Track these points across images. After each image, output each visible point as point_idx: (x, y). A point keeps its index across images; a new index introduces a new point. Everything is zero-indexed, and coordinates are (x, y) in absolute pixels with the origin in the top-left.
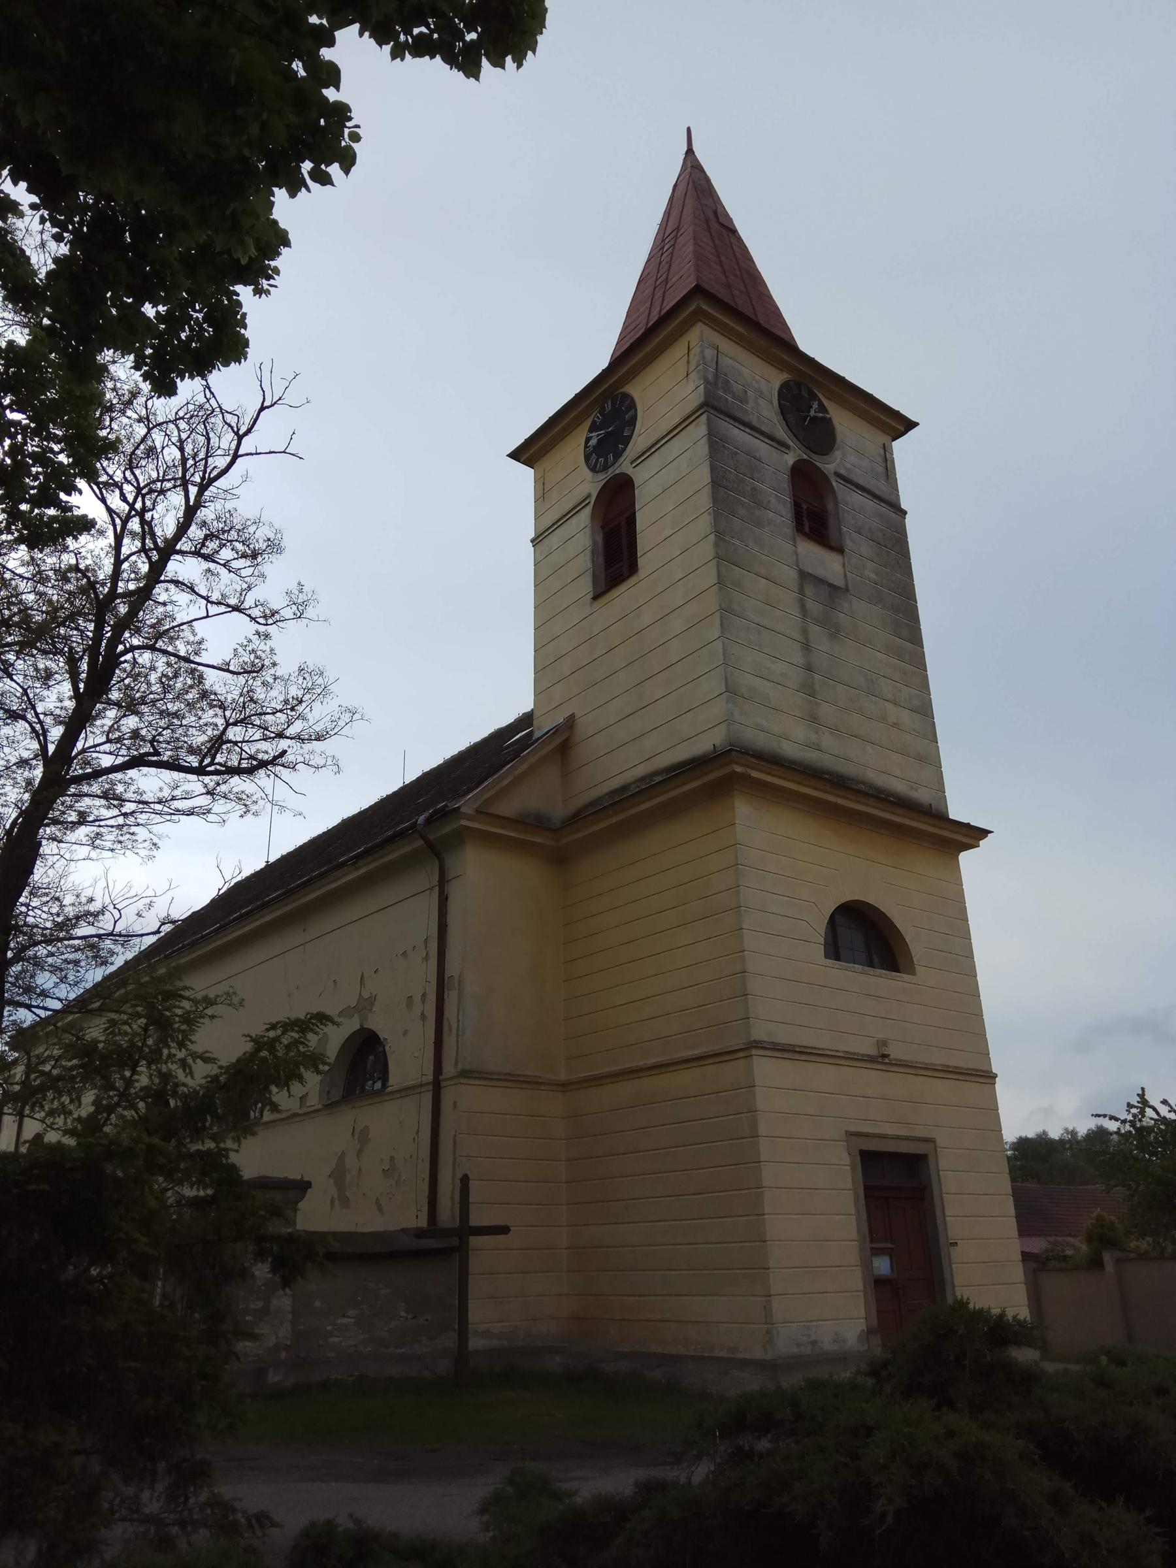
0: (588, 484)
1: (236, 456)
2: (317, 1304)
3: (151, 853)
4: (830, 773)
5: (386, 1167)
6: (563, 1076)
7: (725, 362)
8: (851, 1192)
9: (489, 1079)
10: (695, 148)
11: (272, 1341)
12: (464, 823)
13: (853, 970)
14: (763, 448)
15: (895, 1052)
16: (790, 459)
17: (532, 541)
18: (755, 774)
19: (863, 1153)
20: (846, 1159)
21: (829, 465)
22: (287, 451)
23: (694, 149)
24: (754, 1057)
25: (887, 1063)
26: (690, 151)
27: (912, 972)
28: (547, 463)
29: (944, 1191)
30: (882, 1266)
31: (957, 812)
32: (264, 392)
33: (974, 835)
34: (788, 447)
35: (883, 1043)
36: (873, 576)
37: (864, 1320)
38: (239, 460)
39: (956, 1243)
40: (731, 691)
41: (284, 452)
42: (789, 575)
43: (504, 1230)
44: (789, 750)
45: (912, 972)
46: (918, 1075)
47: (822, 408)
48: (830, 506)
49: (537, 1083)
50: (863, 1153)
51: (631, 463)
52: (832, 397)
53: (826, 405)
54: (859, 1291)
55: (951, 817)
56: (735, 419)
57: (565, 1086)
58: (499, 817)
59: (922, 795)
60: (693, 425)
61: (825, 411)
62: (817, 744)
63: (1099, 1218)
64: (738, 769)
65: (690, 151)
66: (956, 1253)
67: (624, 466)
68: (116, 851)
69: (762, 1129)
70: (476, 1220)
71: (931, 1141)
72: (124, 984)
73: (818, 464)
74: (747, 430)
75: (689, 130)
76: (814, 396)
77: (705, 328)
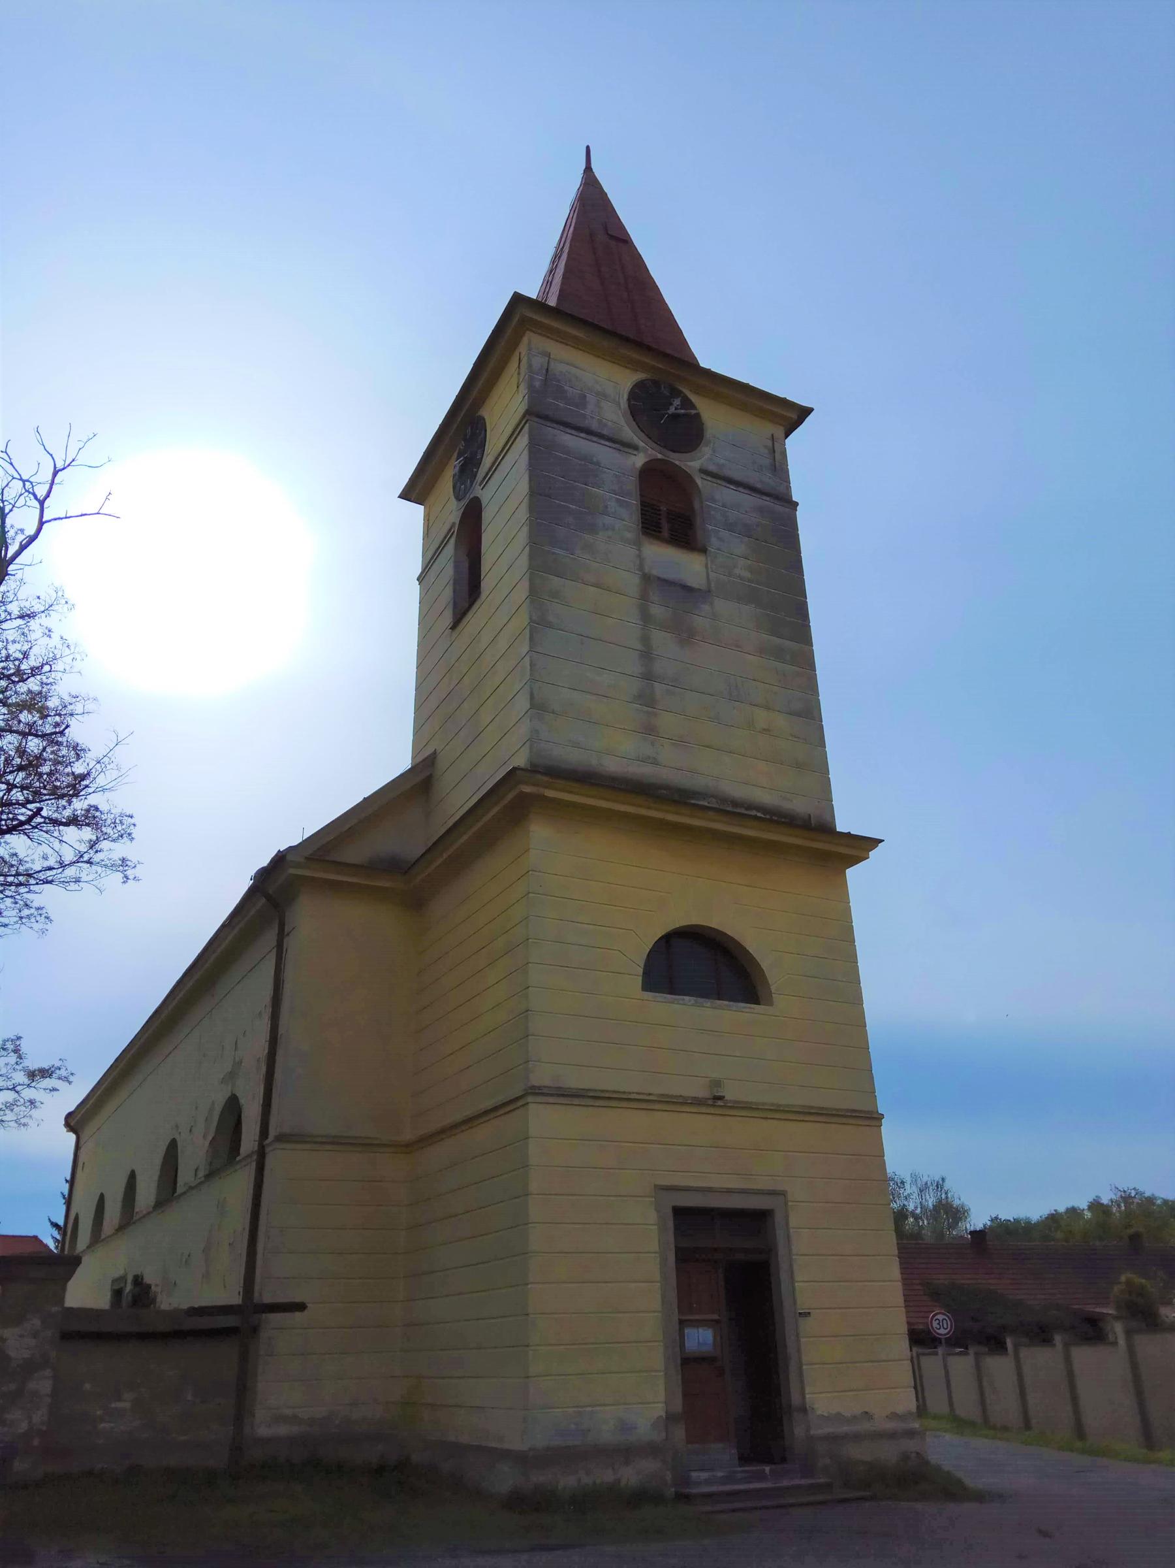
0: (452, 511)
1: (41, 524)
2: (87, 1386)
3: (45, 926)
4: (667, 787)
5: (231, 1242)
6: (408, 1136)
7: (558, 368)
8: (657, 1255)
9: (341, 1144)
10: (593, 166)
11: (24, 1426)
12: (292, 871)
13: (681, 1002)
14: (602, 453)
15: (730, 1093)
16: (639, 460)
17: (418, 580)
18: (550, 793)
19: (680, 1213)
20: (653, 1216)
21: (692, 463)
22: (101, 512)
23: (592, 167)
24: (530, 1104)
25: (721, 1106)
26: (588, 169)
27: (770, 1002)
28: (431, 499)
29: (794, 1251)
30: (701, 1338)
31: (844, 823)
32: (51, 455)
33: (860, 847)
34: (636, 448)
35: (717, 1083)
36: (747, 574)
37: (664, 1405)
38: (45, 526)
39: (809, 1313)
40: (538, 707)
41: (98, 513)
42: (632, 582)
43: (301, 1307)
44: (612, 766)
45: (770, 1002)
46: (767, 1118)
47: (687, 404)
48: (697, 505)
49: (333, 1143)
50: (680, 1213)
51: (480, 485)
52: (699, 390)
53: (693, 400)
54: (660, 1371)
55: (841, 827)
56: (567, 425)
57: (408, 1148)
58: (340, 863)
59: (799, 806)
60: (519, 437)
61: (693, 406)
62: (654, 758)
63: (1129, 1283)
64: (527, 789)
65: (588, 169)
66: (806, 1325)
67: (477, 491)
68: (10, 927)
69: (533, 1187)
70: (267, 1294)
71: (783, 1194)
72: (117, 1067)
73: (677, 463)
74: (583, 435)
75: (588, 148)
76: (676, 393)
77: (532, 334)
